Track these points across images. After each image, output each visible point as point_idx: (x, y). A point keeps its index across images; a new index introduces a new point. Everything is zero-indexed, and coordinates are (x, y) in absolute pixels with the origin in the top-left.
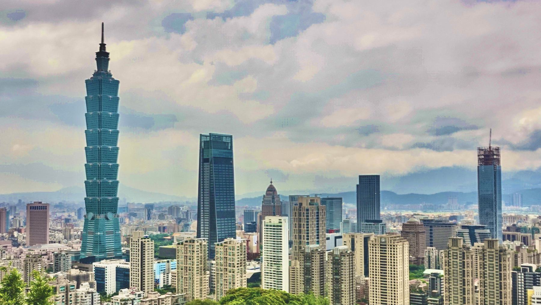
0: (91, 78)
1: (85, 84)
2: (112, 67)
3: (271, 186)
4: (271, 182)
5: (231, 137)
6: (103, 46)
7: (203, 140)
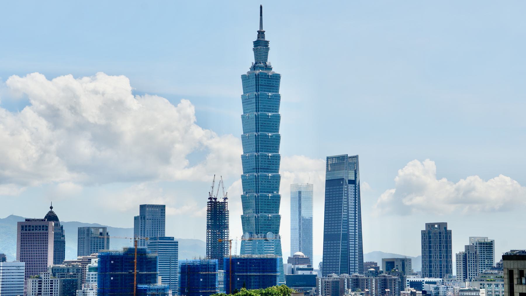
0: (248, 72)
1: (240, 80)
2: (275, 62)
3: (51, 212)
4: (51, 208)
5: (328, 158)
6: (261, 33)
7: (330, 162)
